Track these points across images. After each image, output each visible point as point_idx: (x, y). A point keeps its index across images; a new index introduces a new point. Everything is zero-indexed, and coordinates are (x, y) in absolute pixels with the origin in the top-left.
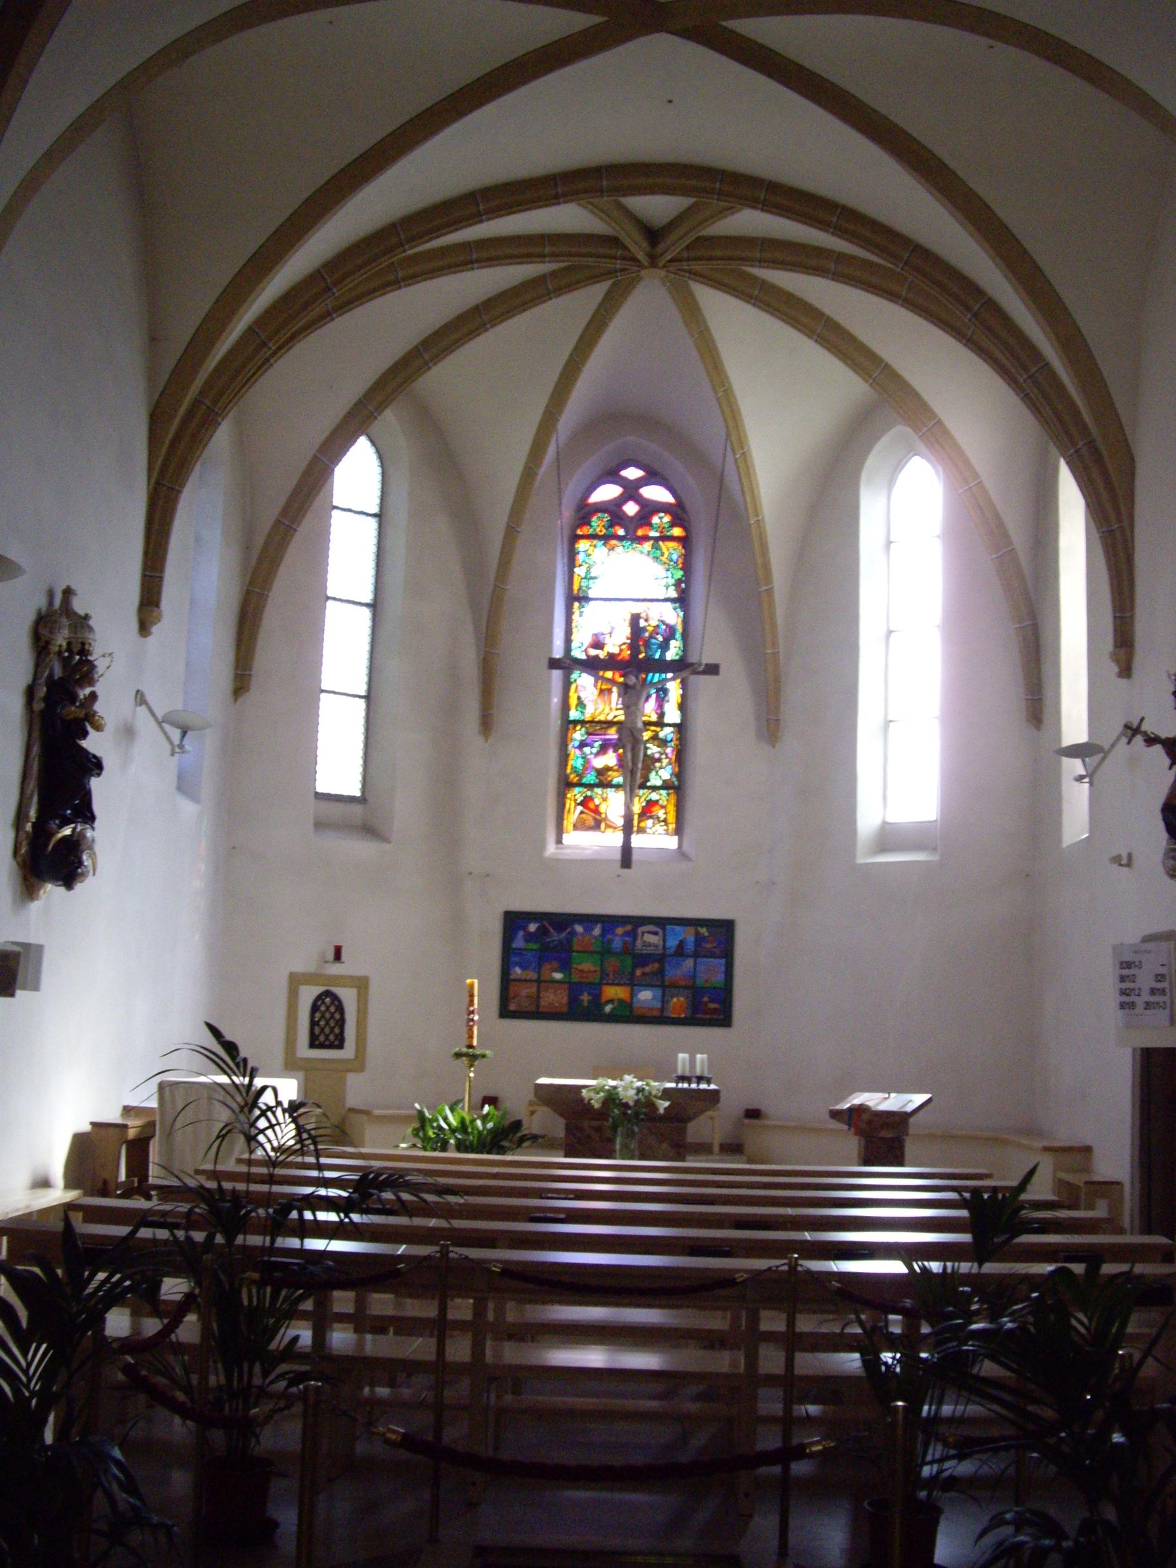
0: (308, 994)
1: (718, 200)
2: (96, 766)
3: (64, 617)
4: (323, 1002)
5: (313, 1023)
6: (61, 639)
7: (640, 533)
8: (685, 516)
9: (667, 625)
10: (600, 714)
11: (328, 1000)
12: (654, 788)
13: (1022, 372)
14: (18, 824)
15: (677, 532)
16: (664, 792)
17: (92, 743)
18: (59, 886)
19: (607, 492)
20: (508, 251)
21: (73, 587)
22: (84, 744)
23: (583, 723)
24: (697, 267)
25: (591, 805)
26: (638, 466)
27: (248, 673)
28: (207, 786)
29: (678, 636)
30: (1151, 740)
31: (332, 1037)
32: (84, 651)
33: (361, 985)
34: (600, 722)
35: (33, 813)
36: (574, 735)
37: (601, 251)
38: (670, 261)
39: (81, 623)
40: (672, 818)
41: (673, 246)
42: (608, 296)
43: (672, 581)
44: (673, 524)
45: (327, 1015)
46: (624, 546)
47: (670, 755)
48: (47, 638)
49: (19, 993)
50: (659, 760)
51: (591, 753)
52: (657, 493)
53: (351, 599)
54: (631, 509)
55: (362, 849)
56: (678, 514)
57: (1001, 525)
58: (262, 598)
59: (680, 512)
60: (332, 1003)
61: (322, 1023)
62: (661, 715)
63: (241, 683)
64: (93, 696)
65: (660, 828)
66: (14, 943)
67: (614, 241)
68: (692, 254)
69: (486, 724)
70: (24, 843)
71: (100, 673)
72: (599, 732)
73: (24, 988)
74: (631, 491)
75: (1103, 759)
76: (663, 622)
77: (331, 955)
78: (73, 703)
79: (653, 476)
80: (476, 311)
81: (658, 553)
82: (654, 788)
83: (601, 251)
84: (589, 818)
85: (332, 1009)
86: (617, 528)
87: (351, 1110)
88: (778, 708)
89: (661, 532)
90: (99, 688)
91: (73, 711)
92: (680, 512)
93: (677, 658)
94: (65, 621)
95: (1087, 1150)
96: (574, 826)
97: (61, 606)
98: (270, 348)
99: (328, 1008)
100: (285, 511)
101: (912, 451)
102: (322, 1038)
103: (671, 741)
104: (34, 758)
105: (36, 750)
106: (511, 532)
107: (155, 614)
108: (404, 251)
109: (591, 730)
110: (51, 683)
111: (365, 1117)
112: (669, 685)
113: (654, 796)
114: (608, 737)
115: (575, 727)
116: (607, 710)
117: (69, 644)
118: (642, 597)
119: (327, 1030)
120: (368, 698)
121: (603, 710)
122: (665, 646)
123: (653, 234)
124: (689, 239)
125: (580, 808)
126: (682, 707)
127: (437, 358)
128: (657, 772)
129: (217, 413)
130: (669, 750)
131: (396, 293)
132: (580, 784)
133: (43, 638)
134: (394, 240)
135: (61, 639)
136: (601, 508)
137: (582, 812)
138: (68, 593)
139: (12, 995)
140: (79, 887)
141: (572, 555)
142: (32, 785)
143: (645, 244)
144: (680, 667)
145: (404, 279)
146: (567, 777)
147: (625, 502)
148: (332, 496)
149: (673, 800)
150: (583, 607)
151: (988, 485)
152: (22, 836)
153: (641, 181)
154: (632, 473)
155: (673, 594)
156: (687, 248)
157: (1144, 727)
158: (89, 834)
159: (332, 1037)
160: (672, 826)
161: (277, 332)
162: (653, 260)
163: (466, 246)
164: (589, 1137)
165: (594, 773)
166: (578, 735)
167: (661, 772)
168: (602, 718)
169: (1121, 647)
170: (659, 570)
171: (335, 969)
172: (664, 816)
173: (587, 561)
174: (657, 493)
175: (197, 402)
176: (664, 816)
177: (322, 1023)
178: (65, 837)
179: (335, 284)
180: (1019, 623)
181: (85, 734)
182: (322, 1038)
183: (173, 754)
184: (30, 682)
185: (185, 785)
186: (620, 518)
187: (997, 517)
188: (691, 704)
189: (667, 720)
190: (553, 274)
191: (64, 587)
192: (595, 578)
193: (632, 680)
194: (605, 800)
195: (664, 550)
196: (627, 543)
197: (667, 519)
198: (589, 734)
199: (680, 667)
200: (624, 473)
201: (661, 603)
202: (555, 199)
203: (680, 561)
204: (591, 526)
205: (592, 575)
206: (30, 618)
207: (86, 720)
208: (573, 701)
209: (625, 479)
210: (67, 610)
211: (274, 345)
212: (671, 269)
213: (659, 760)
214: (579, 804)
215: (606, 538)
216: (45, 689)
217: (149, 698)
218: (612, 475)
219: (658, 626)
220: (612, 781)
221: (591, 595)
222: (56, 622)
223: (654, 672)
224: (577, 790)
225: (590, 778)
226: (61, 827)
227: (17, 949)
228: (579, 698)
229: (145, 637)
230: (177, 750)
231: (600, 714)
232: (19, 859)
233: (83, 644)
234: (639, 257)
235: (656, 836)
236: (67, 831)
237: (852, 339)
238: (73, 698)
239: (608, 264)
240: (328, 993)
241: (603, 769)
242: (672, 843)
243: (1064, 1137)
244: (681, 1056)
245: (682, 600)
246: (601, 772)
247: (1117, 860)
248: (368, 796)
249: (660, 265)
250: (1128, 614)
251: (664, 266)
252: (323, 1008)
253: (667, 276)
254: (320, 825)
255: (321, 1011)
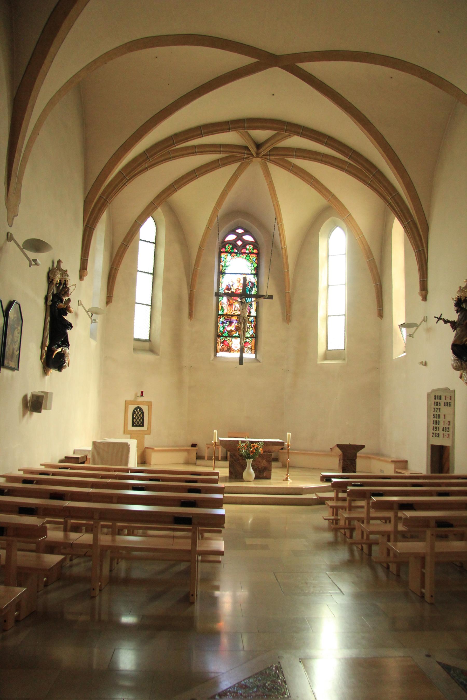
0: (131, 408)
1: (285, 132)
2: (70, 326)
3: (58, 271)
4: (137, 410)
5: (133, 418)
6: (57, 279)
7: (242, 251)
8: (258, 246)
9: (251, 283)
10: (229, 312)
11: (138, 410)
12: (247, 338)
13: (390, 196)
14: (42, 348)
15: (255, 251)
16: (251, 339)
17: (69, 318)
18: (57, 370)
19: (231, 237)
20: (208, 149)
21: (61, 260)
22: (65, 317)
23: (223, 315)
24: (272, 158)
25: (226, 343)
26: (242, 228)
27: (111, 296)
28: (98, 336)
29: (255, 286)
30: (446, 322)
31: (140, 423)
32: (65, 284)
33: (150, 405)
34: (229, 315)
35: (47, 343)
36: (220, 319)
37: (240, 151)
38: (264, 155)
39: (64, 273)
40: (253, 348)
41: (265, 150)
42: (239, 168)
43: (253, 268)
44: (253, 249)
45: (138, 415)
46: (237, 256)
47: (253, 327)
48: (52, 278)
49: (43, 411)
50: (249, 328)
51: (226, 326)
52: (248, 238)
53: (146, 271)
54: (239, 243)
55: (149, 357)
56: (255, 245)
57: (370, 251)
58: (117, 270)
59: (256, 245)
60: (140, 411)
61: (136, 418)
62: (250, 313)
63: (109, 300)
64: (69, 300)
65: (250, 351)
66: (42, 392)
67: (246, 148)
68: (271, 153)
69: (191, 315)
70: (44, 354)
71: (71, 292)
72: (228, 318)
73: (46, 409)
74: (239, 237)
75: (417, 329)
76: (250, 281)
77: (139, 394)
78: (62, 302)
79: (247, 232)
80: (194, 171)
81: (249, 258)
82: (247, 338)
83: (240, 151)
84: (225, 348)
85: (140, 413)
86: (235, 249)
87: (146, 448)
88: (290, 311)
89: (250, 251)
90: (71, 297)
91: (62, 305)
92: (256, 245)
93: (255, 294)
94: (59, 272)
95: (406, 462)
96: (220, 350)
97: (57, 267)
98: (127, 179)
99: (138, 413)
100: (125, 240)
101: (336, 225)
102: (136, 423)
103: (253, 321)
104: (48, 323)
105: (48, 319)
106: (200, 249)
107: (85, 273)
108: (175, 146)
109: (226, 318)
110: (54, 295)
111: (151, 450)
112: (253, 303)
113: (247, 340)
114: (231, 320)
115: (220, 317)
116: (231, 311)
117: (60, 281)
118: (233, 275)
119: (138, 420)
120: (151, 305)
121: (230, 311)
122: (251, 290)
123: (258, 146)
124: (271, 147)
125: (222, 344)
126: (257, 310)
127: (179, 188)
128: (248, 332)
129: (108, 201)
130: (252, 325)
131: (169, 162)
132: (222, 336)
133: (51, 277)
134: (172, 142)
135: (57, 279)
136: (229, 242)
137: (223, 346)
138: (59, 262)
139: (40, 412)
140: (63, 370)
141: (220, 258)
142: (47, 332)
143: (255, 149)
144: (258, 296)
145: (173, 157)
146: (218, 334)
147: (238, 241)
148: (139, 236)
149: (254, 341)
150: (223, 276)
151: (366, 236)
152: (44, 351)
153: (259, 124)
154: (240, 231)
155: (253, 272)
156: (269, 151)
157: (442, 317)
158: (67, 351)
159: (140, 423)
160: (253, 351)
161: (130, 172)
162: (258, 154)
163: (194, 147)
164: (238, 458)
165: (227, 332)
166: (222, 319)
167: (250, 332)
168: (230, 314)
169: (423, 290)
170: (249, 264)
171: (141, 399)
172: (251, 347)
173: (224, 260)
174: (248, 238)
175: (100, 197)
176: (251, 347)
177: (136, 418)
178: (59, 353)
179: (150, 157)
180: (376, 283)
181: (66, 314)
182: (136, 423)
183: (92, 323)
184: (46, 294)
185: (92, 335)
186: (236, 246)
187: (369, 247)
188: (260, 308)
189: (252, 315)
190: (221, 159)
191: (58, 260)
192: (227, 266)
193: (244, 300)
194: (231, 341)
195: (251, 257)
196: (238, 255)
197: (251, 247)
198: (225, 319)
199: (258, 296)
200: (237, 231)
201: (249, 275)
202: (228, 130)
203: (256, 261)
204: (226, 249)
205: (227, 265)
206: (47, 270)
207: (66, 310)
208: (220, 308)
209: (238, 233)
210: (59, 268)
211: (128, 178)
212: (263, 158)
213: (249, 328)
214: (222, 343)
215: (231, 253)
216: (52, 297)
217: (83, 303)
218: (233, 231)
219: (249, 283)
220: (233, 335)
221: (226, 272)
222: (55, 272)
223: (248, 298)
224: (221, 338)
225: (226, 334)
226: (57, 348)
227: (43, 394)
228: (222, 307)
229: (82, 281)
230: (93, 321)
231: (229, 312)
232: (42, 360)
233: (65, 281)
234: (253, 153)
235: (248, 354)
236: (59, 350)
237: (322, 185)
238: (62, 301)
239: (242, 156)
240: (138, 407)
241: (230, 331)
242: (253, 356)
243: (394, 457)
244: (288, 433)
245: (257, 274)
246: (229, 332)
247: (421, 363)
248: (151, 339)
249: (260, 157)
250: (425, 279)
251: (261, 157)
252: (137, 413)
253: (261, 161)
254: (135, 350)
255: (136, 414)
